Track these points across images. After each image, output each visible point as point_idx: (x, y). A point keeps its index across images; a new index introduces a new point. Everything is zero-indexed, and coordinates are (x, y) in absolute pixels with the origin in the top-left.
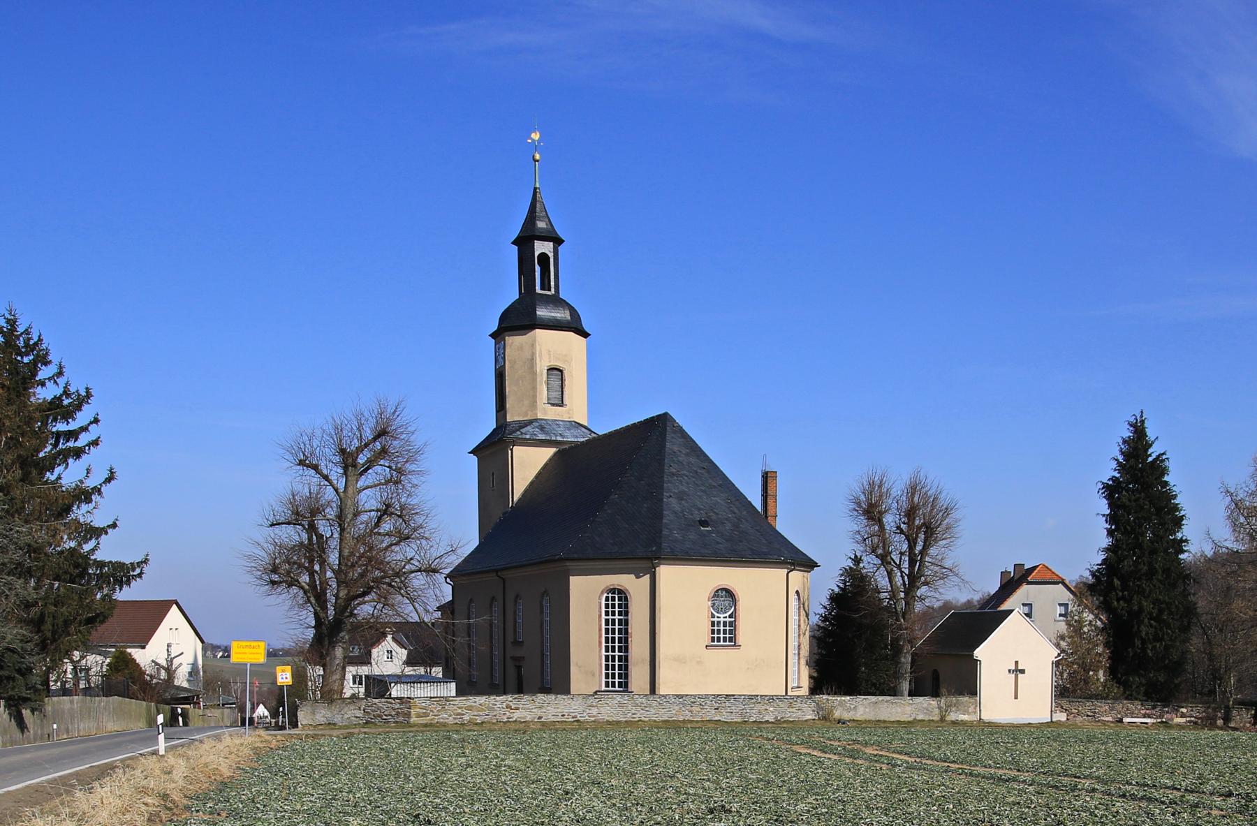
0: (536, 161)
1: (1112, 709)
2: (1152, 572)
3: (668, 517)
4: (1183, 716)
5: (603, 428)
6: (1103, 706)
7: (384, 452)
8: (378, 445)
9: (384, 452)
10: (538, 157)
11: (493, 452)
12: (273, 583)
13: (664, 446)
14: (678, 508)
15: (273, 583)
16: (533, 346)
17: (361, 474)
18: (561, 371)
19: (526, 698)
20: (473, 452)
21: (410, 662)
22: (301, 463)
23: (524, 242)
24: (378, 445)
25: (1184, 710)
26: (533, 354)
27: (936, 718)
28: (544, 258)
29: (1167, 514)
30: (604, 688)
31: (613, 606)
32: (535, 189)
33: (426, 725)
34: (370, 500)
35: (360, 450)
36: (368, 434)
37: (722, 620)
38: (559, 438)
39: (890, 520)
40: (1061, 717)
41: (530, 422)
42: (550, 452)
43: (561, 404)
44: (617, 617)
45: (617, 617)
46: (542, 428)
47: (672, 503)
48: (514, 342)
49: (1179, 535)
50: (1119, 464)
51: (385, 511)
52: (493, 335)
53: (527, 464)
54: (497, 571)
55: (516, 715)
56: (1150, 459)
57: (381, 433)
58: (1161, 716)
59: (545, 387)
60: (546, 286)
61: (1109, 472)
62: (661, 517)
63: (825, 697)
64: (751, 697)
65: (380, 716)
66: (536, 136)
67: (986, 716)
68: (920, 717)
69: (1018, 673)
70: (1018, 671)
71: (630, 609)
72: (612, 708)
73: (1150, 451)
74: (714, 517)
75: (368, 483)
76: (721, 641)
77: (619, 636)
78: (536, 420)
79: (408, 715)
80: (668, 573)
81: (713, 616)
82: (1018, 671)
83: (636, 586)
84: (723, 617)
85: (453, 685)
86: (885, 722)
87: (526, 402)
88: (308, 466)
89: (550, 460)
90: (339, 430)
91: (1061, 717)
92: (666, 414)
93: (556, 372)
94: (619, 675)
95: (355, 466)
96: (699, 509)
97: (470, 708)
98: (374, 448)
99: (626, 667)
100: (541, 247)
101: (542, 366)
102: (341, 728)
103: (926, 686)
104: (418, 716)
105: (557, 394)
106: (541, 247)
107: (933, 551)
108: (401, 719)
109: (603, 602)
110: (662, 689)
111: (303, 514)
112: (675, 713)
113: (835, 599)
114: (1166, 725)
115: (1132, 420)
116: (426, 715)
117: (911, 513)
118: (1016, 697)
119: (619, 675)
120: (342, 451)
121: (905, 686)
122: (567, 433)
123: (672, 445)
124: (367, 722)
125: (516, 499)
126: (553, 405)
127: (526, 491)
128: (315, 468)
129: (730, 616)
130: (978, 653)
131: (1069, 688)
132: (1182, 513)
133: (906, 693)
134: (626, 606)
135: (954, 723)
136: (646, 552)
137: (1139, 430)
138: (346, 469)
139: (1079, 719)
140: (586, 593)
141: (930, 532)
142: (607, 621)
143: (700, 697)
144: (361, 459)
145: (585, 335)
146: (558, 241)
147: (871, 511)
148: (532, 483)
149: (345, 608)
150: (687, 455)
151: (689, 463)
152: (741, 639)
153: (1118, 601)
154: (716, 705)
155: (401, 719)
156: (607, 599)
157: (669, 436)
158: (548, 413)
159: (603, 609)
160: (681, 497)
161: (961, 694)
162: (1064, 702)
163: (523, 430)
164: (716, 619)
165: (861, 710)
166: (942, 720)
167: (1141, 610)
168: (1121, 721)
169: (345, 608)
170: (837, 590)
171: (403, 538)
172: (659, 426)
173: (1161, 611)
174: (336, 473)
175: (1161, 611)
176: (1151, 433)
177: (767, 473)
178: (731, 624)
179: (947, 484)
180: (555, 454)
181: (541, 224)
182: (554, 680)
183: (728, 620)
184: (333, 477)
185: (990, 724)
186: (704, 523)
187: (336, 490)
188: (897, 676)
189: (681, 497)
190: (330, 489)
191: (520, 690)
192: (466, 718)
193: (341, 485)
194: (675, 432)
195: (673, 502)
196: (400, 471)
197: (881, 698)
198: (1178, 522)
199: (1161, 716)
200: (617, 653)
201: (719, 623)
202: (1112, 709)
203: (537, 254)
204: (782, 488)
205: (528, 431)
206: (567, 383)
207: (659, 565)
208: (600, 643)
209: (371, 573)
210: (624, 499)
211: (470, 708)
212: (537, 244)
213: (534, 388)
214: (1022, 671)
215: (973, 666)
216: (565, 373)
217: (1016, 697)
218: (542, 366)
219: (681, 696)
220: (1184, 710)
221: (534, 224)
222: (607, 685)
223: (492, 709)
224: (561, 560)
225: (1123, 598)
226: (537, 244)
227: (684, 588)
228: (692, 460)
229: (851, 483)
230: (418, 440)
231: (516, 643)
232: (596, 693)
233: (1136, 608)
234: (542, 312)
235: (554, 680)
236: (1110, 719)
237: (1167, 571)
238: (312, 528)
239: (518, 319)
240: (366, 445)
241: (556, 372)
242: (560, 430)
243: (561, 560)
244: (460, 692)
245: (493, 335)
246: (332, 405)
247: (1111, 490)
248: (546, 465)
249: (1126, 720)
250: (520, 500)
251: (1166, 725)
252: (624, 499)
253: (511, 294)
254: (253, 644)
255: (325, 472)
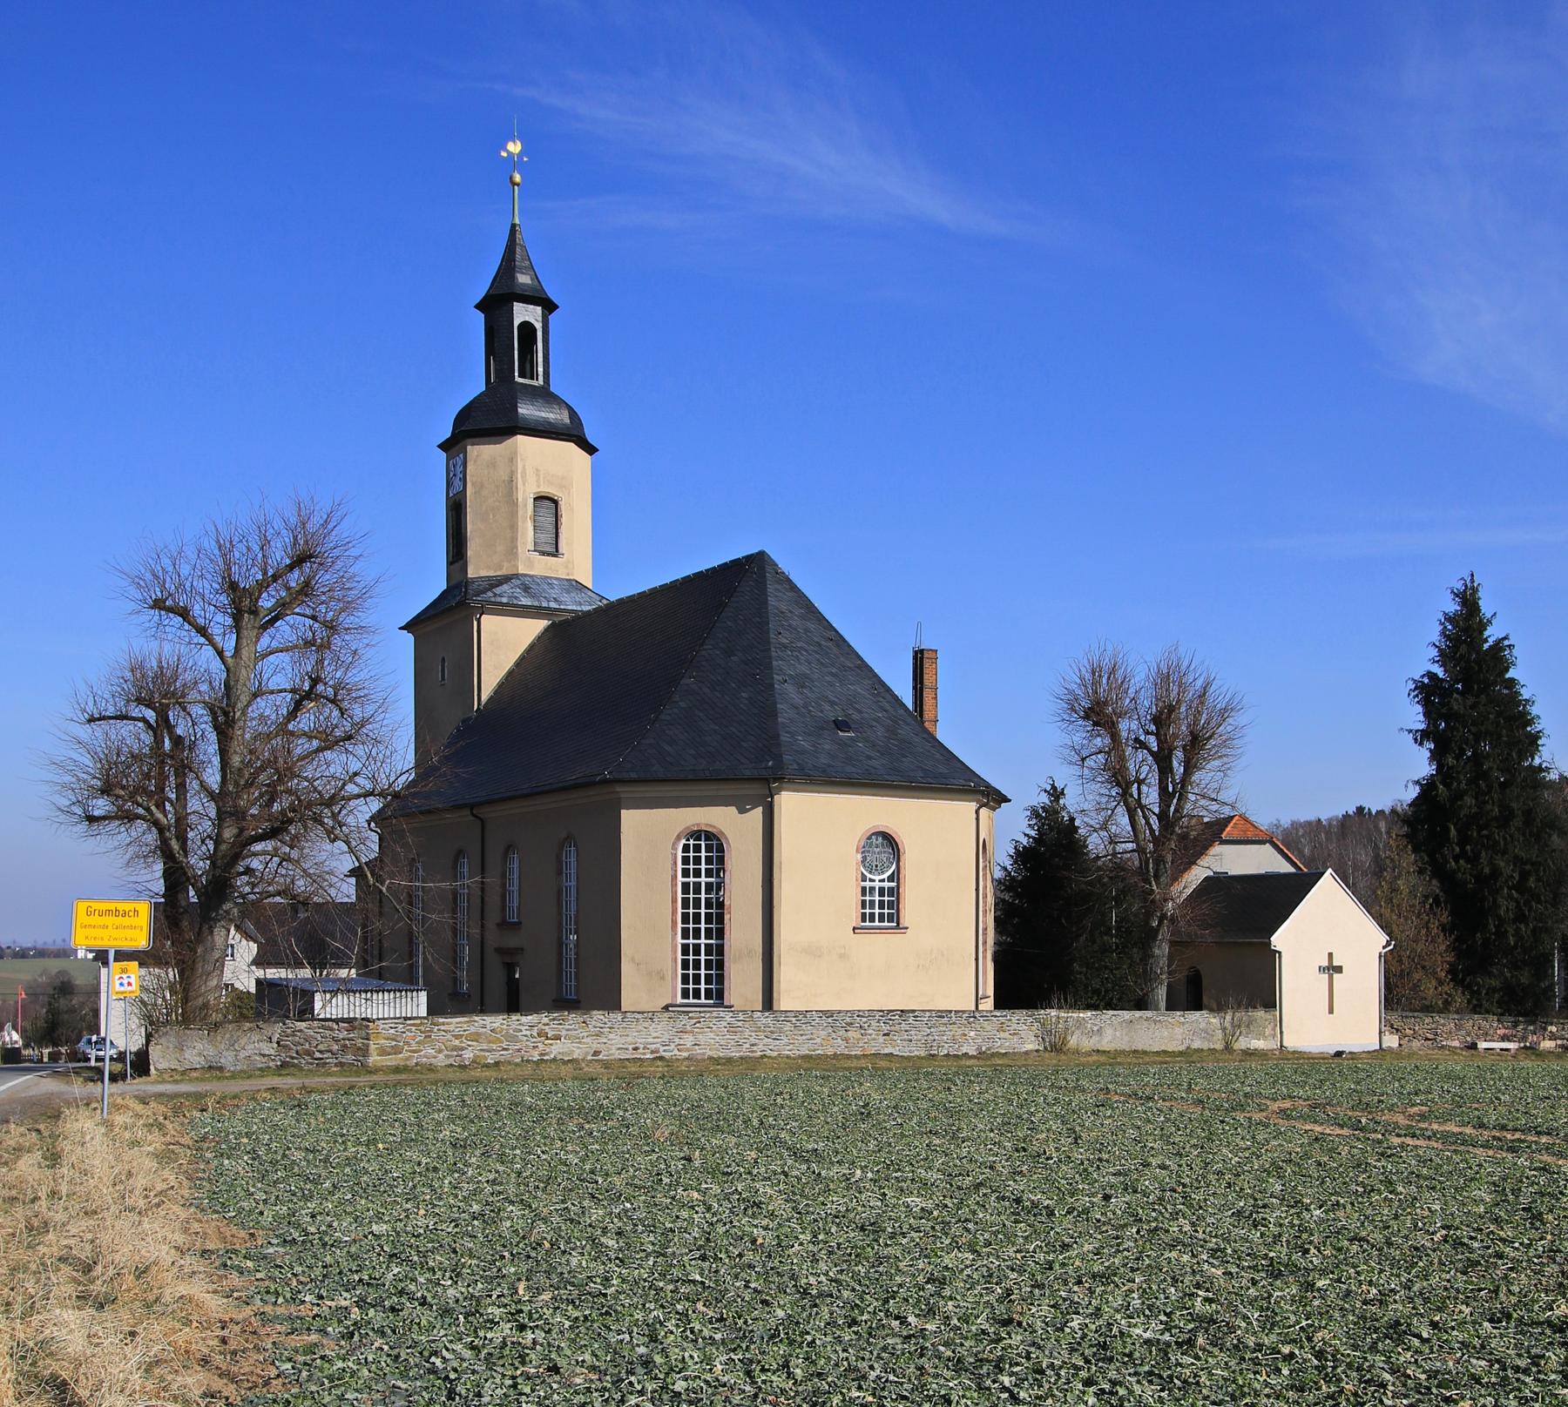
0: (514, 184)
1: (1459, 1027)
2: (1505, 819)
3: (785, 714)
4: (1553, 1037)
5: (616, 592)
6: (1446, 1023)
7: (306, 589)
8: (295, 579)
9: (306, 589)
10: (518, 178)
11: (445, 624)
12: (91, 819)
13: (766, 602)
14: (798, 701)
15: (91, 819)
16: (512, 460)
17: (264, 627)
18: (555, 502)
19: (573, 1018)
20: (407, 627)
21: (259, 962)
22: (158, 604)
23: (496, 304)
24: (295, 579)
25: (1554, 1029)
26: (512, 474)
27: (1219, 1046)
28: (527, 329)
29: (1512, 726)
30: (679, 1000)
31: (697, 860)
32: (513, 226)
33: (397, 1070)
34: (281, 673)
35: (262, 586)
36: (279, 556)
37: (877, 885)
38: (553, 605)
39: (1127, 727)
40: (1392, 1041)
41: (507, 579)
42: (541, 624)
43: (556, 553)
44: (703, 879)
45: (703, 879)
46: (526, 589)
47: (788, 696)
48: (481, 454)
49: (1537, 761)
50: (1440, 650)
51: (302, 697)
52: (444, 446)
53: (503, 643)
54: (472, 807)
55: (556, 1049)
56: (1486, 646)
57: (299, 561)
58: (1524, 1039)
59: (531, 528)
60: (528, 370)
61: (1424, 661)
62: (774, 714)
63: (1054, 1013)
64: (942, 1014)
65: (309, 1053)
66: (514, 148)
67: (1291, 1042)
68: (1196, 1045)
69: (1332, 966)
70: (1332, 969)
71: (728, 864)
72: (711, 1036)
73: (1486, 634)
74: (856, 716)
75: (274, 644)
76: (863, 922)
77: (706, 917)
78: (517, 576)
79: (364, 1051)
80: (789, 803)
81: (864, 879)
82: (1332, 969)
83: (737, 826)
84: (879, 880)
85: (423, 996)
86: (1145, 1052)
87: (500, 548)
88: (170, 610)
89: (539, 638)
90: (225, 551)
91: (1392, 1041)
92: (762, 554)
93: (547, 502)
94: (706, 977)
95: (254, 612)
96: (832, 703)
97: (476, 1037)
98: (282, 586)
99: (720, 965)
100: (524, 313)
101: (526, 492)
102: (234, 1076)
103: (1190, 996)
104: (383, 1052)
105: (547, 537)
106: (524, 313)
107: (1196, 777)
108: (350, 1058)
109: (680, 854)
110: (784, 1002)
111: (156, 695)
112: (822, 1042)
113: (1023, 856)
114: (1531, 1050)
115: (1459, 586)
116: (396, 1050)
117: (1162, 720)
118: (1331, 1011)
119: (706, 977)
120: (233, 586)
121: (1161, 993)
122: (565, 598)
123: (776, 601)
124: (284, 1065)
125: (484, 698)
126: (543, 553)
127: (501, 686)
128: (184, 613)
129: (891, 879)
130: (1278, 940)
131: (1400, 992)
132: (1539, 728)
133: (1163, 1005)
134: (721, 860)
135: (1249, 1054)
136: (757, 772)
137: (1468, 599)
138: (237, 618)
139: (1416, 1044)
140: (650, 838)
141: (1196, 743)
142: (686, 887)
143: (860, 1014)
144: (266, 602)
145: (590, 449)
146: (549, 306)
147: (1098, 713)
148: (510, 673)
149: (227, 862)
150: (802, 617)
151: (807, 630)
152: (907, 918)
153: (1456, 859)
154: (886, 1029)
155: (350, 1058)
156: (686, 848)
157: (770, 588)
158: (534, 565)
159: (680, 866)
160: (801, 682)
161: (1252, 1005)
162: (1394, 1017)
163: (498, 590)
164: (868, 884)
165: (1109, 1032)
166: (1228, 1048)
167: (1496, 873)
168: (1473, 1046)
169: (236, 857)
170: (1025, 841)
171: (329, 741)
172: (750, 573)
173: (1524, 876)
174: (220, 623)
175: (1524, 876)
176: (1486, 607)
177: (922, 651)
178: (891, 890)
179: (1226, 668)
180: (547, 630)
181: (523, 279)
182: (590, 983)
183: (886, 884)
184: (216, 631)
185: (1298, 1055)
186: (841, 725)
187: (220, 653)
188: (1148, 977)
189: (801, 682)
190: (209, 651)
191: (513, 1004)
192: (468, 1055)
193: (229, 645)
194: (779, 582)
195: (789, 688)
196: (331, 627)
197: (1138, 1014)
198: (1533, 742)
199: (1524, 1039)
200: (703, 941)
201: (872, 889)
202: (1459, 1027)
203: (516, 323)
204: (944, 676)
205: (505, 593)
206: (564, 520)
207: (779, 791)
208: (674, 923)
209: (268, 803)
210: (706, 685)
211: (476, 1037)
212: (518, 307)
213: (513, 527)
214: (1339, 969)
215: (1269, 960)
216: (562, 504)
217: (1331, 1011)
218: (526, 492)
219: (828, 1014)
220: (1554, 1029)
221: (513, 278)
222: (685, 994)
223: (513, 1039)
224: (605, 782)
225: (1463, 854)
226: (518, 307)
227: (820, 828)
228: (811, 626)
229: (1064, 671)
230: (364, 571)
231: (504, 925)
232: (666, 1008)
233: (1487, 870)
234: (525, 410)
235: (590, 983)
236: (1456, 1044)
237: (1528, 814)
238: (163, 725)
239: (488, 420)
240: (275, 578)
241: (547, 502)
242: (554, 593)
243: (605, 782)
244: (433, 1010)
245: (444, 446)
246: (222, 505)
247: (1429, 692)
248: (532, 647)
249: (1482, 1045)
250: (491, 699)
251: (1531, 1050)
252: (706, 685)
253: (474, 385)
254: (122, 906)
255: (201, 621)
